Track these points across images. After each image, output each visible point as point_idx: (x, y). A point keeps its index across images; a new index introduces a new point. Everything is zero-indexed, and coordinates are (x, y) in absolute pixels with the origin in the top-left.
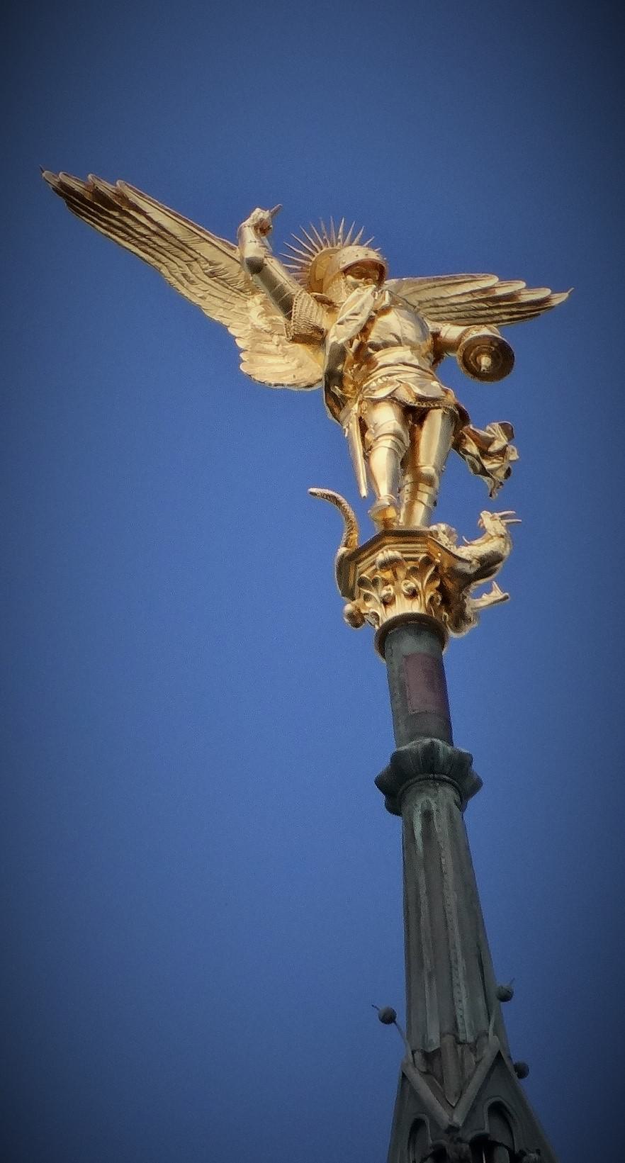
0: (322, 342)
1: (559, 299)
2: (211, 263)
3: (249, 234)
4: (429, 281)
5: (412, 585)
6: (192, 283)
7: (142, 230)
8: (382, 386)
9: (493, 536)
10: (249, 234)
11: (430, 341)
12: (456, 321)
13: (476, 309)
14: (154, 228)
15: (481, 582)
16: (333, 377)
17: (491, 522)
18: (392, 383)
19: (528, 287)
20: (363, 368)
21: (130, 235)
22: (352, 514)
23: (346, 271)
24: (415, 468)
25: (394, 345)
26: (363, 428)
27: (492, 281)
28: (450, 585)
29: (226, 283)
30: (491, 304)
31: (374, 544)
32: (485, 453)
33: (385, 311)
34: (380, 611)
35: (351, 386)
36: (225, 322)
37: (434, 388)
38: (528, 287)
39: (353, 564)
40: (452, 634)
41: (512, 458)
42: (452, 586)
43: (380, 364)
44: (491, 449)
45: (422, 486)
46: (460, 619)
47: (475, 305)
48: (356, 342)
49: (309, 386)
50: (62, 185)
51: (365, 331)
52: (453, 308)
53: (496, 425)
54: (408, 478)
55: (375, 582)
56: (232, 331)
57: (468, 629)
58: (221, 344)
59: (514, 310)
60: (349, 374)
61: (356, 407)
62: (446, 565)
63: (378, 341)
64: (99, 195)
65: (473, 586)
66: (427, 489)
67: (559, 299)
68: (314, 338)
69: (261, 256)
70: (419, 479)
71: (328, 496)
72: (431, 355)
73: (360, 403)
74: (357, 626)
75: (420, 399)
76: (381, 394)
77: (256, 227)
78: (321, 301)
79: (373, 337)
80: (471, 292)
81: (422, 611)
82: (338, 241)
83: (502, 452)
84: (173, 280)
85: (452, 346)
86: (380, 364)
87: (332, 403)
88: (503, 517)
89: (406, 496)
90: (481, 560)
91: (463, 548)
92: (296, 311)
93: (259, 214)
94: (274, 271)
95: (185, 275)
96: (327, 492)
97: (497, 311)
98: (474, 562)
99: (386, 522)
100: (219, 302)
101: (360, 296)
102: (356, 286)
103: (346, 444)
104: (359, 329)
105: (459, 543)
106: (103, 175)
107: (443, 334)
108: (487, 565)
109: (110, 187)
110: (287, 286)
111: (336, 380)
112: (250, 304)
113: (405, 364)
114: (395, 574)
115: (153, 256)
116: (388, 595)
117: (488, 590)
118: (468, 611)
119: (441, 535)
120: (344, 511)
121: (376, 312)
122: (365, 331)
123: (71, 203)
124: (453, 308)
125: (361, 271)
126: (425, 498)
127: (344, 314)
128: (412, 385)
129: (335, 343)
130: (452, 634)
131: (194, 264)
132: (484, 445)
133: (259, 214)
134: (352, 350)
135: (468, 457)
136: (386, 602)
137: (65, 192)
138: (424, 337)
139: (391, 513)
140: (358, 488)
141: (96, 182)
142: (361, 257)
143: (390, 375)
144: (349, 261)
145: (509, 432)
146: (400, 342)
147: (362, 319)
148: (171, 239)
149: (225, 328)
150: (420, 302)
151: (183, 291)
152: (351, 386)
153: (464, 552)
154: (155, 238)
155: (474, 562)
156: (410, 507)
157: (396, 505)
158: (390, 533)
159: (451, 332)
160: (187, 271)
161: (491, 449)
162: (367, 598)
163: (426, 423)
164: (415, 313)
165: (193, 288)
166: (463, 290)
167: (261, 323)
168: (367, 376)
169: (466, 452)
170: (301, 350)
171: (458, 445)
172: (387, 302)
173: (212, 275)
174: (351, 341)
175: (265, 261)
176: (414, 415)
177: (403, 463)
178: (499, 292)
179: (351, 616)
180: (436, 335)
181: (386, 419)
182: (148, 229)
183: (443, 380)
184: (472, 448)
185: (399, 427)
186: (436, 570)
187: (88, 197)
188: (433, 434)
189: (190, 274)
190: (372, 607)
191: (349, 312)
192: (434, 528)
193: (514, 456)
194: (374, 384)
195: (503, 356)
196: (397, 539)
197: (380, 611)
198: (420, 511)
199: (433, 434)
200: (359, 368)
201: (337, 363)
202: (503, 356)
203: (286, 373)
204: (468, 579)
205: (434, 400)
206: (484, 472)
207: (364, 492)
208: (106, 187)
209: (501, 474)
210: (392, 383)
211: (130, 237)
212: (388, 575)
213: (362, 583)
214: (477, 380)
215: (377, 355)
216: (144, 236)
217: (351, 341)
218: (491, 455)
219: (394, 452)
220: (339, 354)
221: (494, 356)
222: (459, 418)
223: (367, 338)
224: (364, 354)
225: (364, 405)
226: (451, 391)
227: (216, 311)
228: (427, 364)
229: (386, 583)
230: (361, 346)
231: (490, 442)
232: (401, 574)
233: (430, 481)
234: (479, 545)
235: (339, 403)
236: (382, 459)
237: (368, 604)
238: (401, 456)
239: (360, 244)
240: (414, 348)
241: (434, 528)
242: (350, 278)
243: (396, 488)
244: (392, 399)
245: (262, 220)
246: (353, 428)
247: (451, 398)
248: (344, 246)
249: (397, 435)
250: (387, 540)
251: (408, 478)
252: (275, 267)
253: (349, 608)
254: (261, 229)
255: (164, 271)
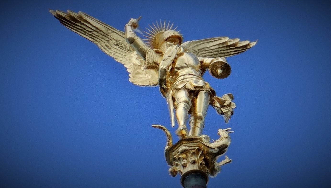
0: (158, 68)
1: (253, 44)
2: (116, 41)
3: (129, 28)
4: (202, 41)
5: (193, 159)
6: (110, 49)
7: (90, 30)
8: (181, 83)
9: (223, 136)
10: (129, 28)
11: (199, 64)
12: (210, 56)
13: (221, 51)
14: (94, 29)
15: (220, 156)
16: (162, 81)
17: (222, 133)
18: (184, 82)
19: (241, 41)
20: (174, 77)
21: (85, 32)
22: (169, 134)
23: (167, 40)
24: (195, 114)
25: (185, 67)
26: (174, 100)
27: (227, 39)
28: (208, 158)
29: (123, 48)
30: (226, 48)
31: (178, 144)
32: (222, 106)
33: (181, 54)
34: (182, 169)
35: (169, 84)
36: (123, 63)
37: (201, 83)
38: (241, 41)
39: (171, 152)
40: (210, 177)
41: (233, 107)
42: (209, 158)
43: (180, 75)
44: (225, 104)
45: (198, 121)
46: (213, 171)
47: (220, 49)
48: (170, 67)
49: (155, 85)
50: (58, 15)
51: (174, 62)
52: (212, 51)
53: (226, 95)
54: (192, 118)
55: (179, 159)
56: (126, 66)
57: (217, 174)
58: (121, 70)
59: (236, 50)
60: (168, 80)
61: (171, 92)
62: (205, 151)
63: (179, 66)
64: (72, 18)
65: (218, 157)
66: (200, 121)
67: (253, 44)
68: (154, 66)
69: (133, 37)
70: (196, 118)
71: (160, 127)
72: (200, 70)
73: (173, 90)
74: (174, 176)
75: (196, 87)
76: (180, 86)
77: (131, 26)
78: (157, 52)
79: (177, 65)
80: (218, 44)
81: (198, 169)
82: (163, 29)
83: (229, 105)
84: (102, 48)
85: (207, 66)
86: (180, 75)
87: (162, 91)
88: (226, 131)
89: (192, 125)
90: (219, 148)
91: (212, 144)
92: (148, 57)
93: (133, 20)
94: (138, 42)
95: (107, 46)
96: (160, 126)
97: (229, 51)
98: (216, 149)
99: (183, 136)
100: (120, 55)
101: (171, 49)
102: (170, 45)
103: (167, 107)
104: (171, 62)
105: (211, 142)
106: (72, 10)
107: (204, 62)
108: (222, 149)
109: (76, 14)
110: (144, 48)
111: (163, 82)
112: (132, 55)
113: (190, 74)
114: (187, 155)
115: (94, 39)
116: (184, 163)
117: (224, 158)
118: (216, 167)
119: (203, 139)
120: (166, 133)
121: (178, 55)
122: (174, 62)
123: (62, 22)
124: (212, 51)
125: (172, 40)
126: (199, 125)
127: (165, 56)
128: (194, 82)
129: (162, 68)
130: (210, 177)
131: (110, 41)
132: (222, 103)
133: (133, 20)
134: (169, 70)
135: (216, 108)
136: (184, 166)
137: (59, 17)
138: (197, 63)
139: (184, 132)
140: (171, 123)
141: (71, 12)
142: (172, 34)
143: (184, 79)
144: (167, 36)
145: (232, 97)
146: (187, 66)
147: (172, 58)
148: (101, 32)
149: (123, 65)
150: (199, 50)
151: (106, 52)
152: (169, 84)
153: (212, 145)
154: (95, 33)
155: (216, 149)
156: (194, 129)
157: (187, 129)
158: (185, 140)
159: (207, 61)
160: (107, 44)
161: (225, 104)
162: (177, 165)
163: (198, 96)
164: (195, 53)
165: (110, 51)
166: (213, 44)
167: (137, 62)
168: (175, 80)
169: (215, 106)
170: (152, 71)
171: (212, 103)
172: (182, 50)
173: (117, 45)
174: (168, 67)
175: (135, 39)
176: (193, 94)
177: (190, 112)
178: (230, 44)
179: (171, 172)
180: (202, 62)
181: (182, 96)
182: (92, 29)
183: (204, 79)
184: (217, 104)
185: (187, 99)
186: (202, 153)
187: (68, 18)
188: (201, 101)
189: (108, 45)
190: (178, 168)
191: (167, 56)
192: (201, 137)
193: (234, 106)
194: (178, 83)
195: (226, 69)
196: (187, 142)
197: (182, 169)
198: (198, 130)
199: (201, 101)
200: (172, 77)
201: (163, 76)
202: (226, 69)
203: (146, 81)
204: (215, 155)
205: (200, 87)
206: (222, 113)
207: (173, 125)
208: (75, 15)
209: (229, 113)
210: (184, 82)
211: (85, 33)
212: (184, 156)
213: (175, 159)
214: (217, 78)
215: (179, 71)
216: (90, 32)
217: (168, 67)
218: (225, 106)
219: (185, 109)
220: (164, 72)
221: (223, 69)
222: (211, 94)
223: (175, 65)
224: (174, 72)
225: (174, 91)
226: (208, 83)
227: (119, 59)
228: (198, 73)
229: (184, 159)
230: (172, 69)
231: (224, 101)
232: (189, 155)
233: (201, 118)
234: (218, 142)
235: (165, 91)
236: (181, 112)
237: (177, 168)
238: (188, 110)
239: (172, 29)
240: (193, 67)
241: (201, 137)
242: (168, 43)
243: (187, 121)
244: (184, 88)
245: (133, 23)
246: (170, 100)
247: (208, 86)
248: (166, 30)
249: (186, 102)
250: (183, 142)
251: (192, 118)
252: (139, 40)
253: (170, 169)
254: (134, 26)
255: (99, 45)
